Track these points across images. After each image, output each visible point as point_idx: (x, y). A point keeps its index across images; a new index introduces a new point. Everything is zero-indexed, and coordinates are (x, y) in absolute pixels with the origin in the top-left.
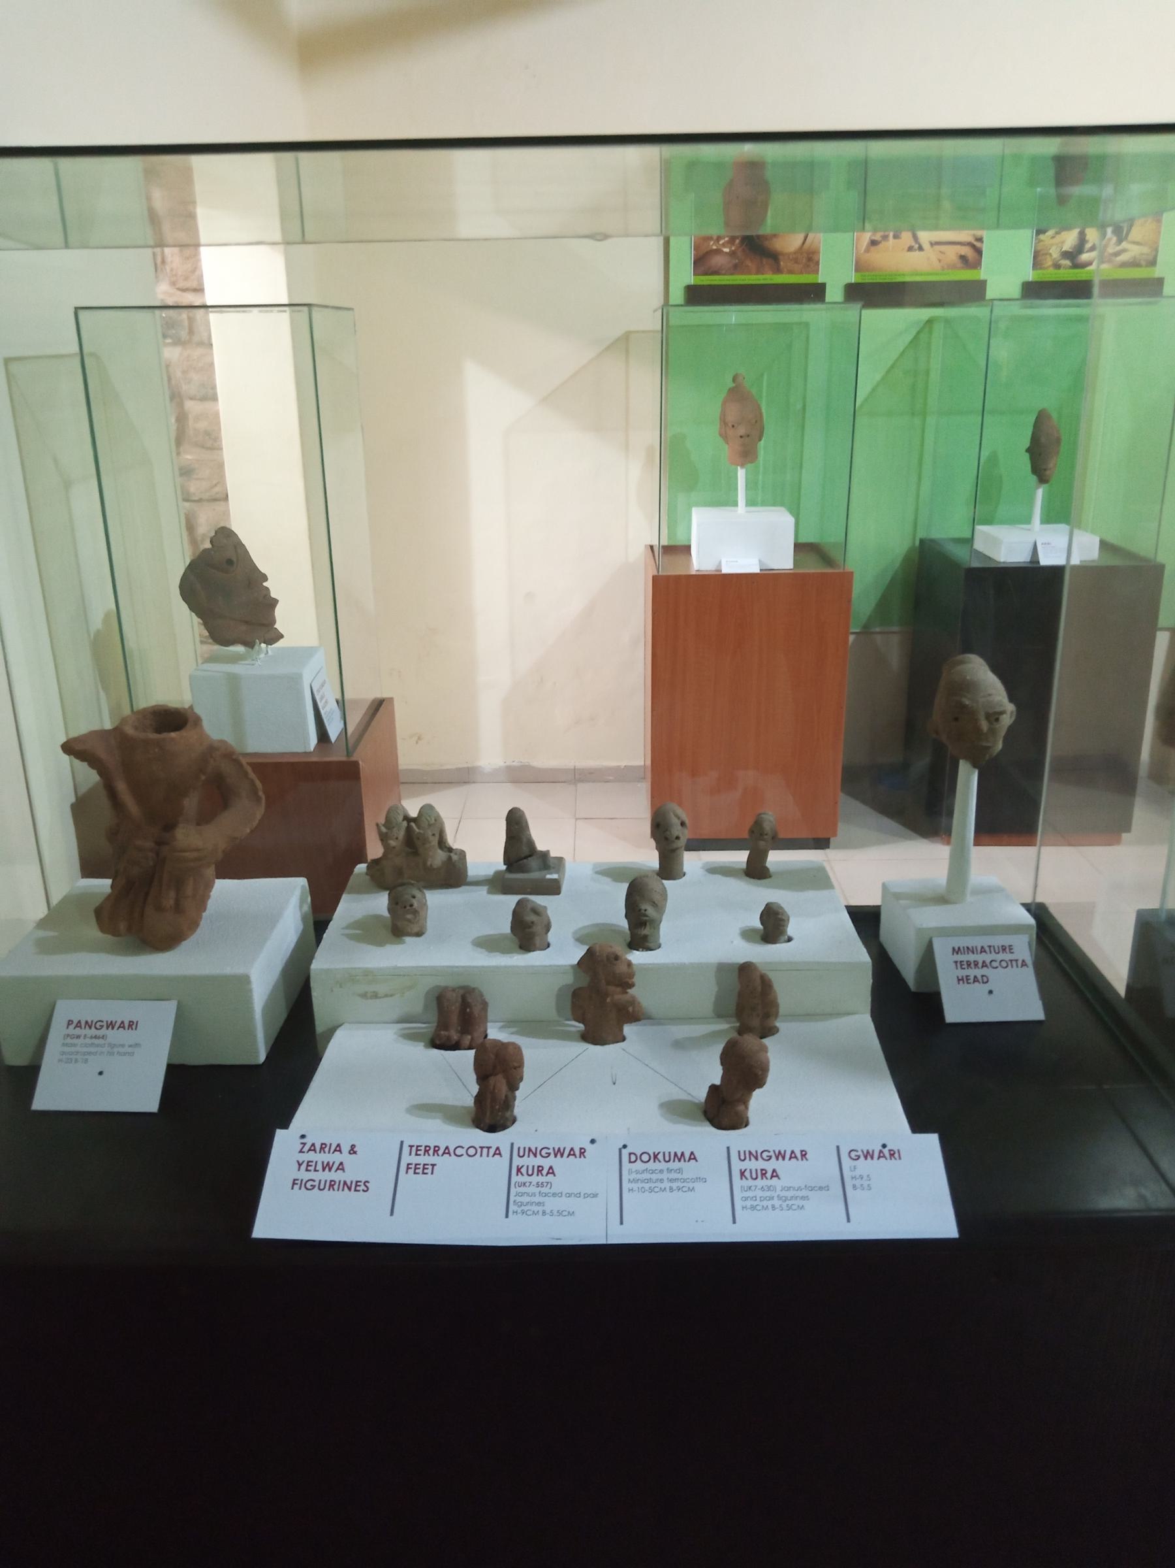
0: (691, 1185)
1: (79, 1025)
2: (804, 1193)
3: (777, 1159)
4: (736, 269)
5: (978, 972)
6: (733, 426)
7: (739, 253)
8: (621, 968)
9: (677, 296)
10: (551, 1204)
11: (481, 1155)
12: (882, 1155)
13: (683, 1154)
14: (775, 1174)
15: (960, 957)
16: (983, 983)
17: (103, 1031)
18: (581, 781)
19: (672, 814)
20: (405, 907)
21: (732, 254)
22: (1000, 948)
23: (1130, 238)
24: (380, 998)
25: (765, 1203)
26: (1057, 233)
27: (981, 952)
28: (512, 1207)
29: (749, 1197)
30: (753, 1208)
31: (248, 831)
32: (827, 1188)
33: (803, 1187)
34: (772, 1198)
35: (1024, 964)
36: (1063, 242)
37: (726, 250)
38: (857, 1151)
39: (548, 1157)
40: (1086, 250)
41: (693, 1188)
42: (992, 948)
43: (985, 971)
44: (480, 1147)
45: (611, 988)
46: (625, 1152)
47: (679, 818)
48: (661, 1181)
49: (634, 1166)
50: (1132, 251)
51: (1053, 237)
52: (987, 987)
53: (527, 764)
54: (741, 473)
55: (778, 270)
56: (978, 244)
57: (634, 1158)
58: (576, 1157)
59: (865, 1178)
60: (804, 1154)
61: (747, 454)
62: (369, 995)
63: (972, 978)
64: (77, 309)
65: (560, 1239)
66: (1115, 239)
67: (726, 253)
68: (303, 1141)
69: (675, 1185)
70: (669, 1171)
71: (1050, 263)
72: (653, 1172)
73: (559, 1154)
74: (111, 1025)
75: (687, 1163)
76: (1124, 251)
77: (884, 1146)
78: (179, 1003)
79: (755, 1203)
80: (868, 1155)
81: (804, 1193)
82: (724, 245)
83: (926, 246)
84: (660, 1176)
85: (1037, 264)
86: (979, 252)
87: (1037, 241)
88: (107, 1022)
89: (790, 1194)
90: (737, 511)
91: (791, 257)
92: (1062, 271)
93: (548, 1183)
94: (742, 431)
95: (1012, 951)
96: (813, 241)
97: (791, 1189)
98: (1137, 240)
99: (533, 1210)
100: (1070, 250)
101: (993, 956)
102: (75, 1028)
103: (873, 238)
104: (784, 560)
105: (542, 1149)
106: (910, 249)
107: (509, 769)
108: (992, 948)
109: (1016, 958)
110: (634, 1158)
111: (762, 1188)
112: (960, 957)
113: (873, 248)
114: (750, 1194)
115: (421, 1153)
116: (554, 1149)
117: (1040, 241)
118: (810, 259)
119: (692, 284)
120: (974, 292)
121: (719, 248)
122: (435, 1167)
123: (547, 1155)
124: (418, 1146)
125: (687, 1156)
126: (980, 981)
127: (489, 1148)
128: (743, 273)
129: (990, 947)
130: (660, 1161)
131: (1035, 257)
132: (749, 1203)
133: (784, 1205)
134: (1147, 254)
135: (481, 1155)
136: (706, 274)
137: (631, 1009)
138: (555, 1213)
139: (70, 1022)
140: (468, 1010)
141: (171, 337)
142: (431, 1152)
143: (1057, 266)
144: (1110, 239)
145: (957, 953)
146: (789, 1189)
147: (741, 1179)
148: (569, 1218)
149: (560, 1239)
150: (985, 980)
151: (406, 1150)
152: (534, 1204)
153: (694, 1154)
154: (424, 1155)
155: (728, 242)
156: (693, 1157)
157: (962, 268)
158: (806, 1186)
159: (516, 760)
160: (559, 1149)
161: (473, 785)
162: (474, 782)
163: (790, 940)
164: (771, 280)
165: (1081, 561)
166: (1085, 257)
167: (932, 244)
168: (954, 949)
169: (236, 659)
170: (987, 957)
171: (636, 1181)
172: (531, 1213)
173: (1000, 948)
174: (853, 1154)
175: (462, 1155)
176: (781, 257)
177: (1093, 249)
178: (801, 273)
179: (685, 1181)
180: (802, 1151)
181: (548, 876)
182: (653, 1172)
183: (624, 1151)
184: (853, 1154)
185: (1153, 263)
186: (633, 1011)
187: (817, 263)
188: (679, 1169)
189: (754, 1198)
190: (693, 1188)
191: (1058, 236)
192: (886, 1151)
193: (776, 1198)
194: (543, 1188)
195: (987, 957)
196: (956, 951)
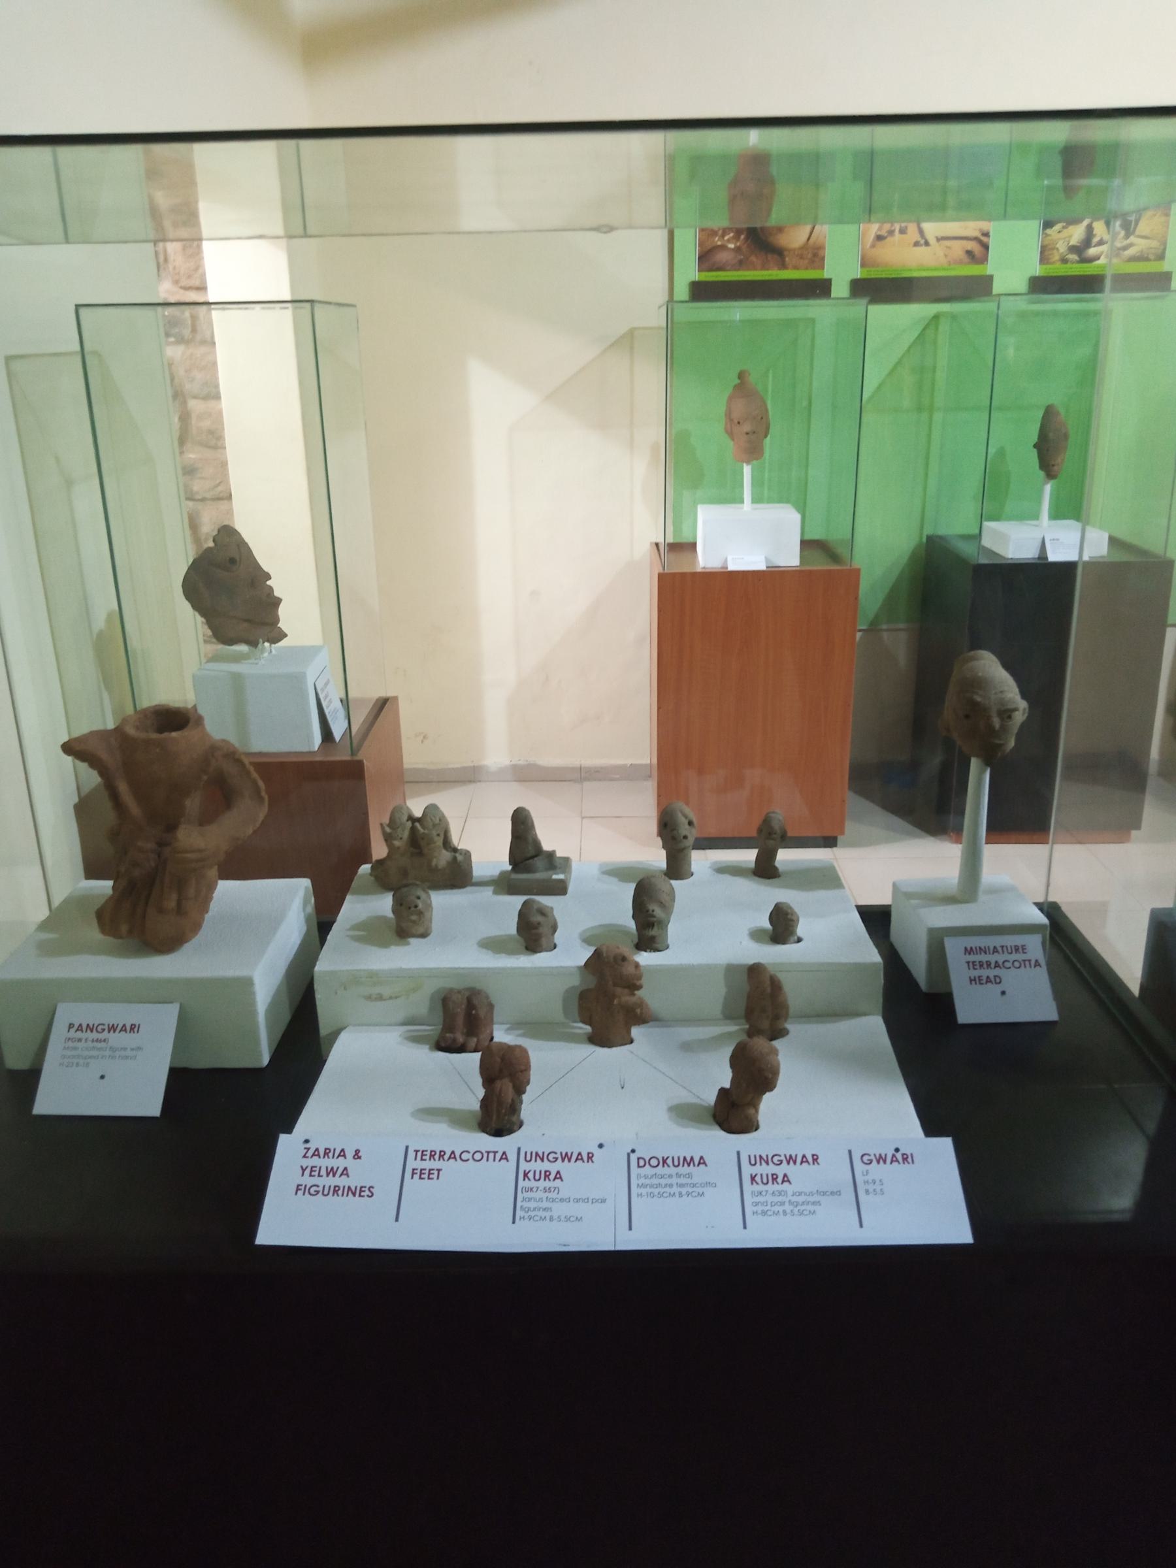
1: (453, 1156)
2: (816, 1198)
4: (741, 265)
5: (992, 973)
6: (739, 423)
9: (682, 292)
10: (559, 1209)
11: (488, 1160)
14: (786, 1179)
15: (971, 958)
16: (996, 983)
17: (105, 1035)
21: (738, 250)
23: (1137, 233)
24: (385, 1000)
26: (1064, 228)
28: (519, 1213)
30: (764, 1213)
32: (839, 1193)
34: (783, 1204)
35: (1037, 964)
36: (1070, 237)
38: (780, 1156)
39: (866, 1164)
40: (1093, 244)
43: (997, 972)
44: (486, 1152)
45: (619, 990)
46: (633, 1157)
48: (671, 1186)
49: (642, 1171)
50: (1139, 245)
51: (1059, 232)
52: (999, 988)
54: (747, 470)
55: (783, 266)
56: (984, 239)
57: (643, 1162)
58: (583, 1162)
59: (878, 1182)
61: (752, 450)
63: (984, 979)
64: (9, 359)
66: (1123, 233)
68: (307, 1145)
69: (684, 1191)
71: (1057, 257)
74: (112, 1028)
76: (1131, 245)
79: (766, 1209)
80: (881, 1159)
81: (816, 1198)
82: (728, 241)
83: (932, 241)
84: (669, 1181)
85: (1044, 259)
86: (986, 247)
87: (1044, 236)
88: (109, 1025)
89: (801, 1199)
90: (742, 508)
91: (796, 253)
92: (1069, 265)
94: (747, 427)
95: (1025, 951)
98: (1144, 234)
100: (1079, 244)
102: (76, 1031)
103: (879, 233)
104: (790, 558)
106: (916, 244)
108: (1005, 948)
110: (643, 1162)
111: (773, 1193)
112: (971, 958)
113: (879, 243)
116: (561, 1153)
117: (1047, 235)
118: (815, 255)
120: (979, 287)
123: (554, 1160)
124: (423, 1151)
126: (994, 982)
127: (495, 1153)
128: (748, 269)
129: (1002, 947)
130: (668, 1166)
131: (1042, 253)
132: (760, 1208)
133: (796, 1210)
134: (1155, 248)
135: (488, 1160)
136: (710, 270)
137: (638, 1011)
138: (563, 1218)
139: (71, 1026)
140: (474, 1012)
142: (437, 1157)
143: (1064, 261)
144: (1119, 233)
146: (800, 1194)
150: (998, 980)
151: (411, 1154)
155: (733, 238)
156: (702, 1161)
157: (969, 263)
160: (566, 1154)
161: (478, 783)
162: (480, 781)
163: (799, 940)
165: (1090, 557)
166: (1092, 251)
167: (939, 239)
168: (966, 949)
169: (238, 658)
170: (1000, 958)
174: (866, 1159)
176: (786, 253)
177: (1101, 243)
178: (807, 268)
179: (694, 1185)
180: (813, 1155)
181: (555, 877)
184: (866, 1159)
185: (1161, 257)
186: (641, 1013)
187: (823, 259)
190: (703, 1193)
191: (1065, 231)
192: (899, 1156)
195: (1000, 958)
196: (968, 951)
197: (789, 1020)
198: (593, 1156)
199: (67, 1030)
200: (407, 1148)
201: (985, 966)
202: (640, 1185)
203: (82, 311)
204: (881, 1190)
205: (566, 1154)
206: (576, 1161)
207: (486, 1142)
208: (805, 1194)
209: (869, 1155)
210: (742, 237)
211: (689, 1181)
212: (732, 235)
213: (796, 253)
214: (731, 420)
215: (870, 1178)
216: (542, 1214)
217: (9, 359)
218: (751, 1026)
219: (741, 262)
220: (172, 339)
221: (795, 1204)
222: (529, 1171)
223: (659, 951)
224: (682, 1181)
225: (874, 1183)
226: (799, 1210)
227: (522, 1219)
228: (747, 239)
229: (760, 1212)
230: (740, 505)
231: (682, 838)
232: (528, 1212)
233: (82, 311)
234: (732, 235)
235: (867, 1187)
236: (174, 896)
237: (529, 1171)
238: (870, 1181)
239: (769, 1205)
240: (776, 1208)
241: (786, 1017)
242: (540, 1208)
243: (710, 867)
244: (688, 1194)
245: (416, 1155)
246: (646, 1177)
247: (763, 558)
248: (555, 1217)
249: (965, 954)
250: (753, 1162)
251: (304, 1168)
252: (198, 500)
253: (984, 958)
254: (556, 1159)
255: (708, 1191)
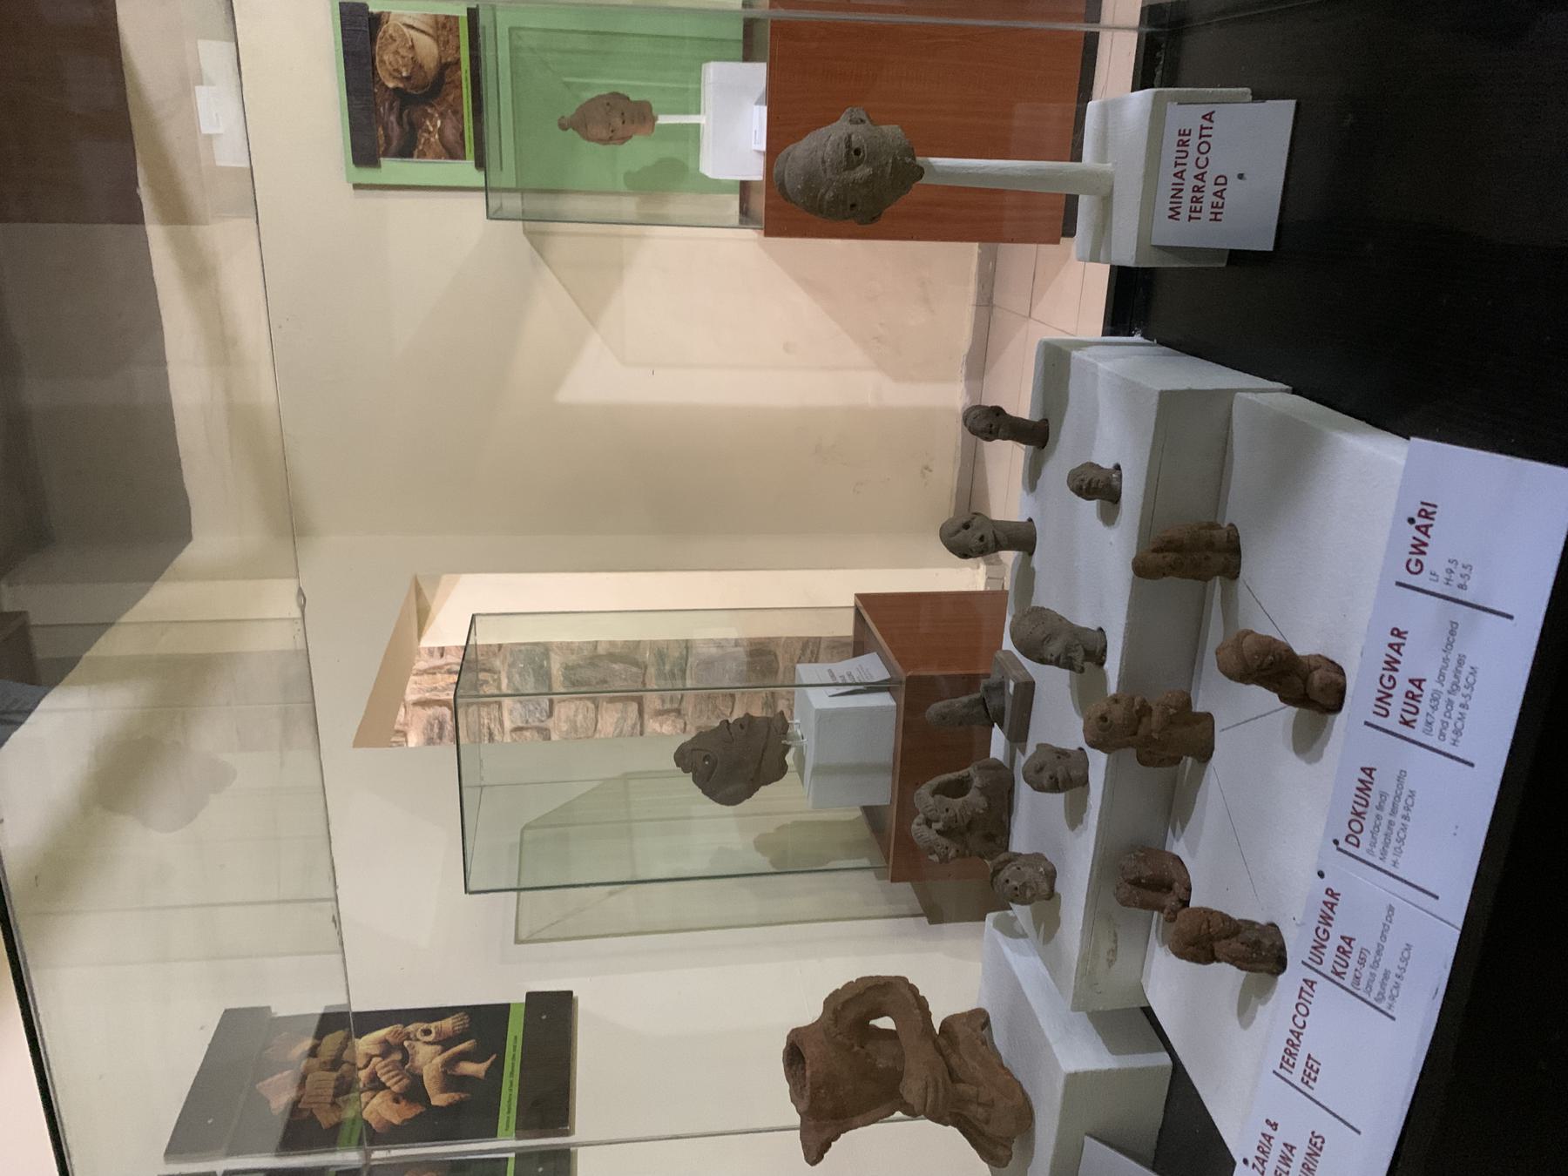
0: (1405, 793)
1: (1423, 529)
2: (1453, 657)
3: (1423, 553)
4: (458, 112)
5: (1210, 188)
7: (442, 109)
8: (1118, 712)
10: (1390, 961)
12: (1200, 177)
13: (1361, 781)
14: (1418, 682)
15: (1184, 212)
16: (1226, 184)
18: (991, 298)
19: (955, 538)
20: (1017, 895)
21: (442, 115)
22: (1180, 148)
24: (1116, 947)
25: (1455, 714)
27: (1181, 178)
28: (1383, 1006)
29: (1441, 731)
30: (1458, 732)
31: (918, 1011)
32: (1454, 625)
33: (1444, 655)
34: (1450, 703)
35: (1208, 117)
37: (439, 123)
39: (1422, 566)
41: (1190, 131)
42: (1179, 161)
43: (1209, 179)
45: (1142, 731)
46: (1343, 845)
47: (958, 531)
48: (1391, 823)
49: (1365, 844)
52: (1232, 180)
53: (965, 358)
54: (663, 120)
55: (457, 62)
57: (1353, 837)
59: (1451, 566)
60: (1397, 633)
62: (1111, 958)
63: (1217, 200)
64: (518, 941)
65: (1437, 990)
67: (442, 123)
68: (1250, 1164)
69: (1401, 811)
70: (1380, 808)
72: (1377, 826)
73: (1422, 548)
75: (1374, 782)
77: (1411, 521)
78: (1091, 1136)
79: (1451, 727)
80: (1419, 547)
81: (1453, 657)
82: (434, 126)
84: (1384, 823)
89: (1449, 674)
91: (443, 49)
93: (1361, 952)
94: (617, 122)
95: (1187, 132)
96: (427, 24)
97: (1443, 671)
99: (1467, 674)
101: (1190, 161)
104: (757, 74)
105: (1381, 683)
107: (970, 376)
108: (1179, 161)
109: (1199, 128)
110: (1353, 837)
111: (1433, 708)
112: (1184, 212)
114: (1437, 726)
115: (1198, 206)
116: (1411, 553)
118: (444, 26)
119: (473, 162)
121: (437, 130)
122: (1312, 1056)
123: (1419, 565)
125: (1364, 777)
126: (1223, 187)
129: (1176, 164)
132: (1449, 733)
133: (1464, 691)
137: (1172, 711)
140: (1143, 881)
141: (542, 661)
142: (1199, 195)
145: (1178, 213)
146: (1442, 674)
147: (1413, 727)
148: (1479, 675)
149: (1437, 990)
150: (1221, 181)
151: (1282, 1072)
152: (1459, 669)
153: (1366, 768)
154: (1295, 1059)
156: (1369, 771)
158: (1445, 651)
159: (960, 371)
160: (1387, 662)
163: (1118, 467)
164: (466, 72)
168: (1170, 217)
169: (801, 759)
170: (1191, 171)
171: (1384, 853)
172: (1471, 677)
173: (1180, 148)
174: (1412, 567)
175: (1207, 159)
176: (443, 61)
179: (1398, 796)
181: (1011, 690)
182: (1377, 826)
183: (1340, 846)
184: (1412, 567)
186: (1176, 708)
187: (447, 17)
188: (1381, 796)
189: (1445, 725)
190: (1472, 668)
192: (1420, 521)
193: (1451, 697)
194: (1367, 959)
195: (1191, 171)
196: (1174, 214)
197: (1219, 521)
198: (1397, 629)
199: (1411, 729)
200: (1274, 1072)
201: (1199, 195)
202: (1382, 857)
203: (472, 887)
204: (1463, 567)
205: (1387, 662)
206: (1429, 537)
207: (1288, 982)
208: (1445, 668)
209: (1409, 561)
210: (429, 111)
211: (1390, 801)
212: (428, 123)
213: (443, 49)
214: (611, 138)
215: (1443, 575)
216: (1390, 983)
217: (518, 941)
218: (1218, 574)
219: (455, 112)
220: (545, 663)
221: (1455, 687)
222: (1402, 716)
223: (1106, 646)
224: (1388, 807)
225: (1452, 572)
226: (1465, 687)
227: (1450, 582)
228: (432, 106)
229: (1454, 736)
230: (702, 126)
231: (981, 544)
232: (1458, 687)
233: (472, 887)
234: (428, 123)
235: (1454, 584)
236: (973, 1107)
237: (1402, 716)
238: (1447, 576)
239: (1449, 721)
240: (1455, 714)
241: (1213, 526)
242: (1456, 669)
243: (1028, 494)
244: (1407, 808)
245: (1285, 1068)
246: (1373, 844)
247: (756, 108)
248: (1398, 972)
249: (1178, 219)
250: (1384, 712)
251: (1363, 816)
252: (687, 652)
253: (1187, 195)
254: (1391, 678)
255: (1409, 784)
